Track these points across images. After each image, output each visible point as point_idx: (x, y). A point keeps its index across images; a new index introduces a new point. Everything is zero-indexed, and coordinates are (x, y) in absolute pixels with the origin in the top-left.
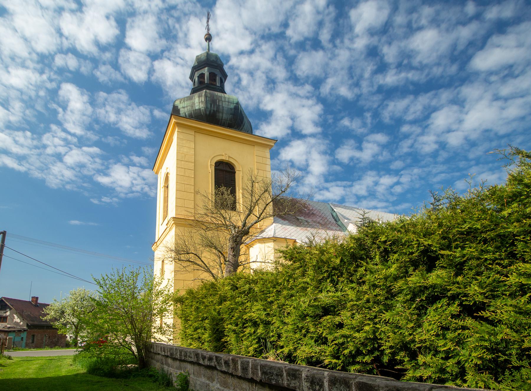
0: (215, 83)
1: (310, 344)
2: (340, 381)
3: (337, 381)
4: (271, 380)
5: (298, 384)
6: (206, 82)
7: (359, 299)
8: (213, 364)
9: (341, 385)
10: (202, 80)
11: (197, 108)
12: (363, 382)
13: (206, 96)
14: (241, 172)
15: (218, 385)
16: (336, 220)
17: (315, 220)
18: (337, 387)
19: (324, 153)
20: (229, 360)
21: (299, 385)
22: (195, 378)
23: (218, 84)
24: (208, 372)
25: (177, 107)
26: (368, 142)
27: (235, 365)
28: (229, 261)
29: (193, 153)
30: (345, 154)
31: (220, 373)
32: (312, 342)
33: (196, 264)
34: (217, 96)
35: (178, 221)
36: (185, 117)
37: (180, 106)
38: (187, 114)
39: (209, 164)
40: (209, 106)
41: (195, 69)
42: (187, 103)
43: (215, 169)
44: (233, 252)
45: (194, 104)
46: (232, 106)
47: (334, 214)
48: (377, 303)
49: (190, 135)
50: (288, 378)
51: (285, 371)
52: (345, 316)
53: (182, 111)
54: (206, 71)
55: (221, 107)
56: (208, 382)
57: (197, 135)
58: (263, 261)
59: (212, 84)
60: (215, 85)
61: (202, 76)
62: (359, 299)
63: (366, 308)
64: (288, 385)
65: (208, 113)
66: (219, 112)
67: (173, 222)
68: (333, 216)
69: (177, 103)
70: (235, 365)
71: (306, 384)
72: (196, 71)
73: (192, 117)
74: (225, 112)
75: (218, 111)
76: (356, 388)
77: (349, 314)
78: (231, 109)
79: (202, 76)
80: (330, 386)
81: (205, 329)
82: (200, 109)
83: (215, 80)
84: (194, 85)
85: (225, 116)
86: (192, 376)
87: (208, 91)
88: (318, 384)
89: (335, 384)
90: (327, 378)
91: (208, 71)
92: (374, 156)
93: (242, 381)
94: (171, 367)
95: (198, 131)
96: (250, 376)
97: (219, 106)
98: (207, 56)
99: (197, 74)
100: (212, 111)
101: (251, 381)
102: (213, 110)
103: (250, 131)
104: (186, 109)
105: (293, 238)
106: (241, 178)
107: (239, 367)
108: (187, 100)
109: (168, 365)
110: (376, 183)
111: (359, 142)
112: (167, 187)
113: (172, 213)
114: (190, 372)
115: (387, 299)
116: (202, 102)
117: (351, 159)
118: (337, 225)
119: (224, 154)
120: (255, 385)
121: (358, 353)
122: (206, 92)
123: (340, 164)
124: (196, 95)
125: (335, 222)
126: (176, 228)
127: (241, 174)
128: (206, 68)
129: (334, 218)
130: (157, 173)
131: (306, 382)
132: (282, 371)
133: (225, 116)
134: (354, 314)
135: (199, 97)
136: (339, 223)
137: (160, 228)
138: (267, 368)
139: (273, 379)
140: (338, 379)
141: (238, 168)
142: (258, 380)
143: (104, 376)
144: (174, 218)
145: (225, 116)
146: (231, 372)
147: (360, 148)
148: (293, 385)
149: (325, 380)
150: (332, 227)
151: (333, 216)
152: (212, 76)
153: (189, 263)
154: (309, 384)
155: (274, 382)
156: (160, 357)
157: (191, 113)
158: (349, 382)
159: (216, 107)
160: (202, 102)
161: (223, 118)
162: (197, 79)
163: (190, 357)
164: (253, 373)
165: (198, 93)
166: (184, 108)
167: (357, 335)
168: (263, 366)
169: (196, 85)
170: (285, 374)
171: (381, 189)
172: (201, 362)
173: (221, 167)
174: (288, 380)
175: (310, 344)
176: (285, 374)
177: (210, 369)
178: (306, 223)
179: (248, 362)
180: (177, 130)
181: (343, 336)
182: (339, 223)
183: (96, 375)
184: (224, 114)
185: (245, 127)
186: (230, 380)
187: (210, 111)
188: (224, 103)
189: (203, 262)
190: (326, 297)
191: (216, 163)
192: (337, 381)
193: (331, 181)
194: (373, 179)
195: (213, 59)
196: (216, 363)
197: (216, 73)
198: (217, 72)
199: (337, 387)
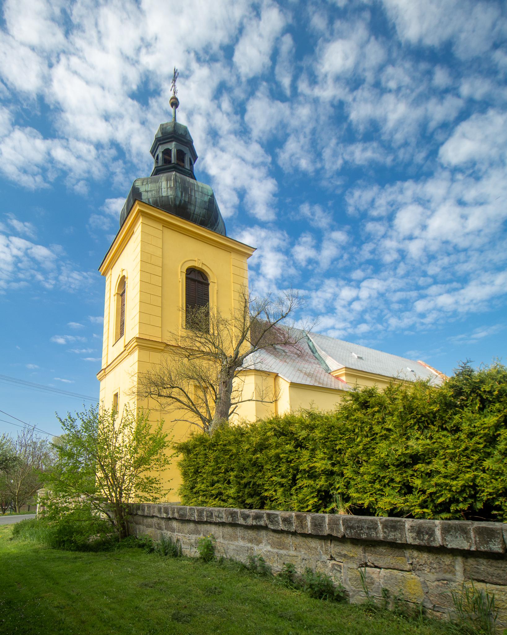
0: (182, 164)
1: (392, 494)
2: (455, 528)
3: (451, 528)
4: (359, 534)
5: (399, 535)
6: (173, 162)
7: (455, 447)
8: (262, 523)
9: (457, 532)
10: (167, 157)
11: (164, 194)
12: (483, 527)
13: (176, 181)
14: (216, 284)
15: (269, 548)
16: (312, 352)
17: (292, 350)
18: (451, 535)
19: (278, 249)
20: (291, 517)
21: (401, 537)
22: (226, 542)
23: (187, 166)
24: (251, 534)
25: (138, 189)
26: (330, 239)
27: (301, 522)
28: (220, 398)
29: (161, 254)
30: (303, 252)
31: (271, 534)
32: (395, 492)
33: (180, 401)
34: (189, 182)
35: (143, 343)
36: (149, 204)
37: (142, 189)
38: (151, 200)
39: (179, 271)
40: (179, 194)
41: (159, 141)
42: (149, 187)
43: (187, 278)
44: (226, 387)
45: (160, 188)
46: (206, 199)
47: (311, 344)
48: (476, 451)
49: (156, 230)
50: (385, 530)
51: (381, 523)
52: (437, 464)
53: (145, 196)
54: (173, 146)
55: (193, 198)
56: (250, 545)
57: (166, 230)
58: (260, 399)
59: (180, 165)
60: (183, 167)
61: (167, 152)
62: (455, 447)
63: (463, 456)
64: (385, 538)
65: (178, 203)
66: (191, 204)
67: (136, 344)
68: (309, 346)
69: (138, 184)
70: (301, 522)
71: (410, 534)
72: (160, 144)
73: (158, 206)
74: (198, 204)
75: (189, 202)
76: (474, 533)
77: (442, 462)
78: (205, 202)
79: (167, 152)
80: (443, 533)
81: (229, 483)
82: (168, 196)
83: (183, 161)
84: (157, 162)
85: (198, 210)
86: (220, 540)
87: (178, 174)
88: (427, 533)
89: (449, 532)
90: (440, 526)
91: (176, 145)
92: (334, 260)
93: (310, 540)
94: (179, 532)
95: (167, 225)
96: (326, 531)
97: (191, 196)
98: (174, 127)
99: (161, 149)
100: (183, 201)
101: (330, 538)
102: (185, 201)
103: (223, 233)
104: (150, 194)
105: (275, 371)
106: (215, 292)
107: (309, 524)
108: (151, 183)
109: (173, 530)
110: (335, 296)
111: (319, 238)
112: (122, 294)
113: (132, 330)
114: (216, 536)
115: (485, 446)
116: (170, 187)
117: (310, 261)
118: (314, 358)
119: (196, 259)
120: (329, 542)
121: (454, 500)
122: (176, 175)
123: (295, 264)
124: (163, 177)
125: (312, 353)
126: (139, 351)
127: (216, 287)
128: (174, 143)
129: (310, 349)
130: (105, 274)
131: (411, 532)
132: (376, 524)
133: (197, 210)
134: (446, 462)
135: (167, 180)
136: (316, 355)
137: (110, 349)
138: (353, 522)
139: (363, 534)
140: (452, 526)
141: (212, 279)
142: (340, 535)
143: (76, 551)
144: (137, 338)
145: (198, 210)
146: (293, 530)
147: (318, 247)
148: (393, 537)
149: (437, 528)
150: (310, 360)
151: (309, 346)
152: (181, 155)
153: (169, 400)
154: (414, 535)
155: (364, 536)
156: (155, 520)
157: (156, 200)
158: (466, 528)
159: (187, 196)
160: (170, 187)
161: (196, 213)
162: (161, 155)
163: (218, 517)
164: (331, 529)
165: (166, 175)
166: (148, 191)
167: (455, 483)
168: (347, 520)
169: (160, 163)
170: (380, 527)
171: (339, 305)
172: (241, 521)
173: (192, 276)
174: (385, 532)
175: (392, 494)
176: (380, 527)
177: (253, 529)
178: (284, 354)
179: (324, 517)
180: (141, 220)
181: (437, 485)
182: (316, 355)
183: (64, 549)
184: (196, 207)
185: (219, 227)
186: (289, 540)
187: (181, 201)
188: (197, 193)
189: (189, 399)
190: (417, 444)
191: (187, 270)
192: (451, 528)
193: (286, 288)
194: (331, 290)
195: (181, 132)
196: (267, 522)
197: (185, 152)
198: (186, 150)
199: (451, 535)
